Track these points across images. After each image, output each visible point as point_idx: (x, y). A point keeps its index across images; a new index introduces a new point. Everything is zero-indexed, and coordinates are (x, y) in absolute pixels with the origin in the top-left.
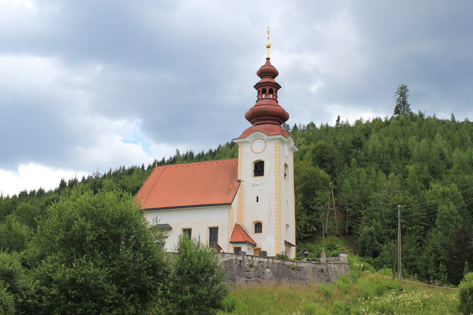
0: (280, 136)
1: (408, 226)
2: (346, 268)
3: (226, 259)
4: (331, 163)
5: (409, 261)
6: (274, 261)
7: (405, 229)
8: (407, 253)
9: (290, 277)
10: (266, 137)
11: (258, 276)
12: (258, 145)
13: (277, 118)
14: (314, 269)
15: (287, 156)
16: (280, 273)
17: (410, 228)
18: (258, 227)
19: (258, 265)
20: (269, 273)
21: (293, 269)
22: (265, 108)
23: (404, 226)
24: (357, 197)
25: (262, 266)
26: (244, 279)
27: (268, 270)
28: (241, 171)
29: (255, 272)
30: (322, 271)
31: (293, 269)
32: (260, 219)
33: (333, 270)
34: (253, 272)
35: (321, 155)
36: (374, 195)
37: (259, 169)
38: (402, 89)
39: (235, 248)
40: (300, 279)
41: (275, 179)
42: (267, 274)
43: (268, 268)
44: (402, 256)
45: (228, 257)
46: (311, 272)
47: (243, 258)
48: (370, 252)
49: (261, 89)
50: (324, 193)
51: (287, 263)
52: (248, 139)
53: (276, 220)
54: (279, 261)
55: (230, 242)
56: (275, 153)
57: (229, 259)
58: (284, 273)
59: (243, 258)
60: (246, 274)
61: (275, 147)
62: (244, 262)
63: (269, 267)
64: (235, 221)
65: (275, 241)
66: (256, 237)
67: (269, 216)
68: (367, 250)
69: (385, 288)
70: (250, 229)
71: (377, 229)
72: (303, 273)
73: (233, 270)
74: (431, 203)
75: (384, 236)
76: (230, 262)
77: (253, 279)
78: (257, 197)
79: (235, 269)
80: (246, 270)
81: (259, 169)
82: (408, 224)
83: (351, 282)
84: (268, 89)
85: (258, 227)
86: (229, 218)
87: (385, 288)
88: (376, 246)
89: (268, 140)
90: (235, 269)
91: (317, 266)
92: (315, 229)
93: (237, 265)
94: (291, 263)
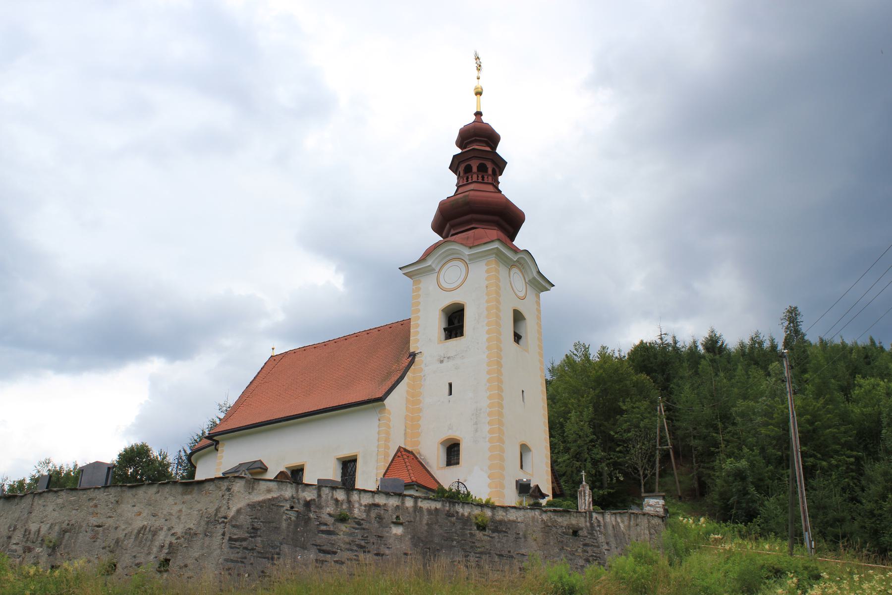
0: (496, 245)
1: (819, 459)
2: (654, 527)
3: (261, 498)
4: (663, 372)
5: (831, 526)
6: (420, 504)
7: (814, 467)
8: (825, 507)
9: (468, 548)
10: (466, 252)
11: (361, 547)
12: (452, 273)
13: (496, 218)
14: (547, 528)
15: (522, 294)
16: (436, 540)
17: (824, 463)
18: (452, 451)
19: (364, 516)
20: (399, 538)
21: (482, 527)
22: (465, 196)
23: (812, 459)
24: (707, 411)
25: (380, 518)
26: (312, 555)
27: (398, 531)
28: (417, 333)
29: (351, 534)
30: (575, 533)
31: (482, 527)
33: (610, 531)
34: (346, 534)
35: (643, 361)
36: (741, 405)
38: (791, 313)
40: (501, 556)
41: (489, 340)
42: (391, 541)
43: (397, 524)
44: (813, 517)
45: (269, 491)
46: (539, 535)
47: (319, 496)
48: (738, 510)
49: (461, 169)
50: (637, 404)
51: (464, 511)
52: (429, 262)
53: (491, 432)
54: (438, 505)
56: (487, 282)
57: (269, 496)
58: (450, 539)
59: (319, 496)
60: (318, 542)
61: (487, 271)
62: (320, 507)
63: (402, 520)
64: (398, 441)
65: (489, 481)
67: (476, 424)
68: (734, 511)
69: (764, 573)
70: (434, 457)
71: (752, 465)
72: (512, 537)
73: (277, 528)
74: (862, 413)
75: (769, 482)
76: (272, 504)
77: (344, 555)
78: (450, 385)
79: (284, 525)
80: (323, 528)
81: (454, 322)
82: (819, 455)
83: (664, 562)
84: (475, 165)
85: (452, 451)
86: (379, 433)
87: (764, 573)
88: (754, 501)
89: (474, 258)
90: (284, 525)
91: (560, 520)
92: (622, 479)
93: (293, 515)
94: (477, 511)
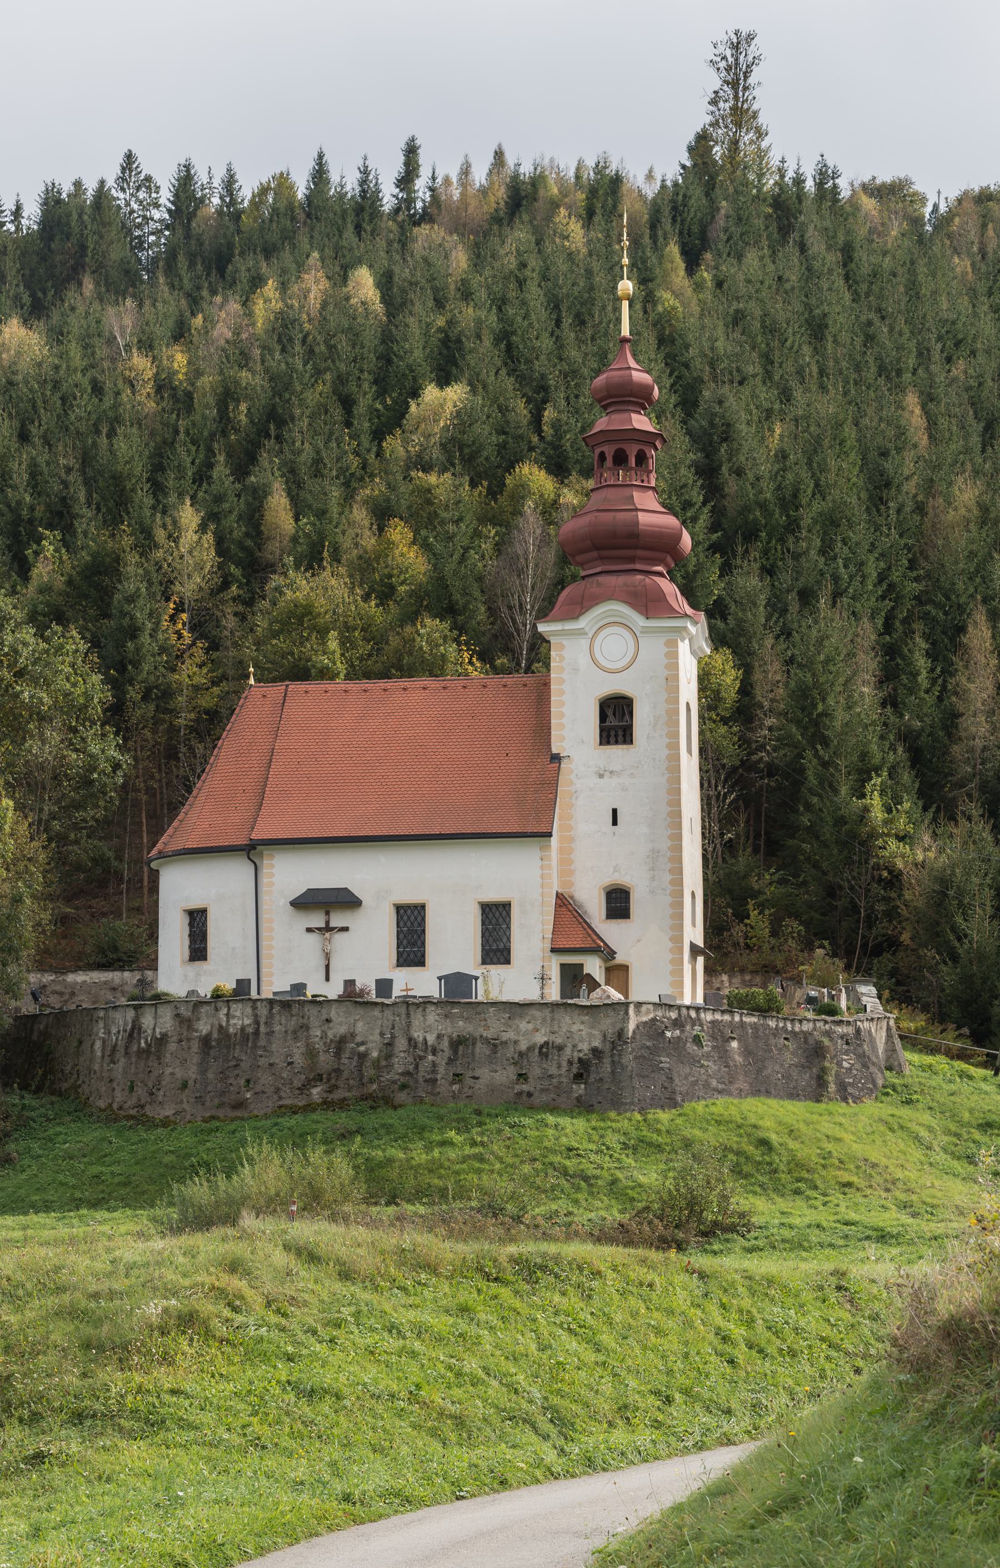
10: (639, 621)
18: (618, 903)
32: (623, 879)
37: (612, 721)
39: (563, 966)
55: (553, 950)
66: (612, 932)
70: (595, 907)
78: (615, 812)
81: (616, 720)
89: (646, 631)
